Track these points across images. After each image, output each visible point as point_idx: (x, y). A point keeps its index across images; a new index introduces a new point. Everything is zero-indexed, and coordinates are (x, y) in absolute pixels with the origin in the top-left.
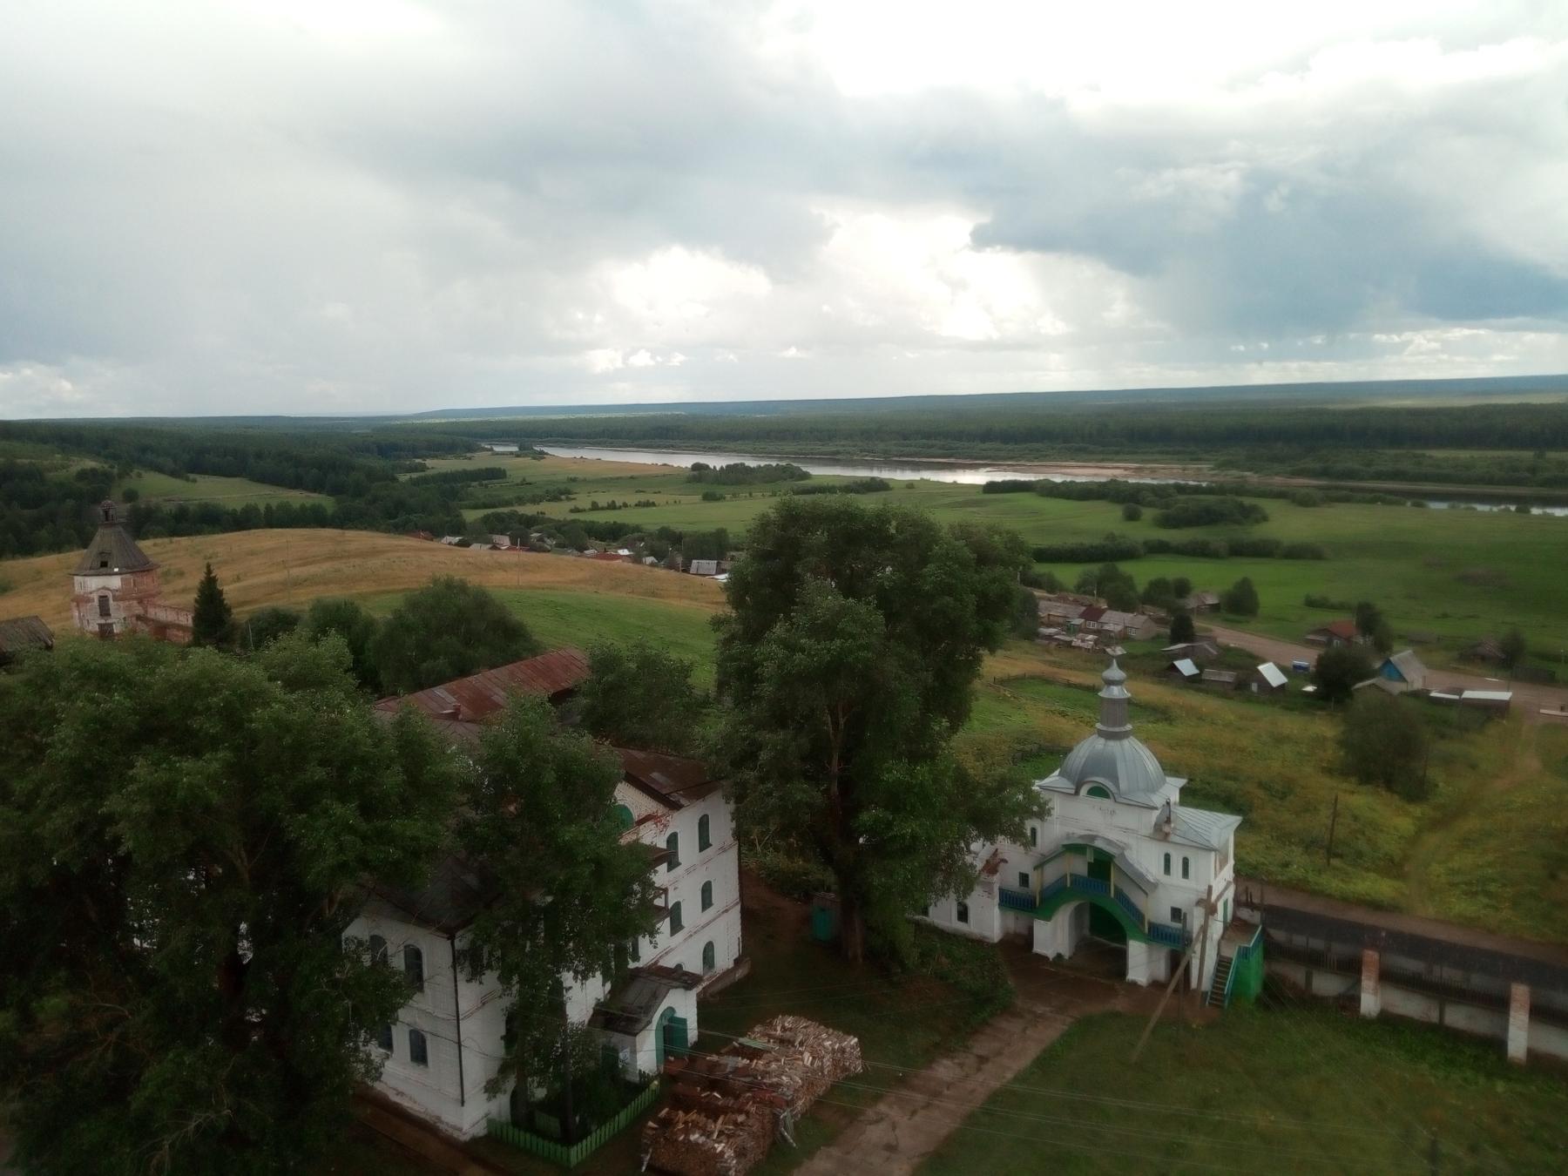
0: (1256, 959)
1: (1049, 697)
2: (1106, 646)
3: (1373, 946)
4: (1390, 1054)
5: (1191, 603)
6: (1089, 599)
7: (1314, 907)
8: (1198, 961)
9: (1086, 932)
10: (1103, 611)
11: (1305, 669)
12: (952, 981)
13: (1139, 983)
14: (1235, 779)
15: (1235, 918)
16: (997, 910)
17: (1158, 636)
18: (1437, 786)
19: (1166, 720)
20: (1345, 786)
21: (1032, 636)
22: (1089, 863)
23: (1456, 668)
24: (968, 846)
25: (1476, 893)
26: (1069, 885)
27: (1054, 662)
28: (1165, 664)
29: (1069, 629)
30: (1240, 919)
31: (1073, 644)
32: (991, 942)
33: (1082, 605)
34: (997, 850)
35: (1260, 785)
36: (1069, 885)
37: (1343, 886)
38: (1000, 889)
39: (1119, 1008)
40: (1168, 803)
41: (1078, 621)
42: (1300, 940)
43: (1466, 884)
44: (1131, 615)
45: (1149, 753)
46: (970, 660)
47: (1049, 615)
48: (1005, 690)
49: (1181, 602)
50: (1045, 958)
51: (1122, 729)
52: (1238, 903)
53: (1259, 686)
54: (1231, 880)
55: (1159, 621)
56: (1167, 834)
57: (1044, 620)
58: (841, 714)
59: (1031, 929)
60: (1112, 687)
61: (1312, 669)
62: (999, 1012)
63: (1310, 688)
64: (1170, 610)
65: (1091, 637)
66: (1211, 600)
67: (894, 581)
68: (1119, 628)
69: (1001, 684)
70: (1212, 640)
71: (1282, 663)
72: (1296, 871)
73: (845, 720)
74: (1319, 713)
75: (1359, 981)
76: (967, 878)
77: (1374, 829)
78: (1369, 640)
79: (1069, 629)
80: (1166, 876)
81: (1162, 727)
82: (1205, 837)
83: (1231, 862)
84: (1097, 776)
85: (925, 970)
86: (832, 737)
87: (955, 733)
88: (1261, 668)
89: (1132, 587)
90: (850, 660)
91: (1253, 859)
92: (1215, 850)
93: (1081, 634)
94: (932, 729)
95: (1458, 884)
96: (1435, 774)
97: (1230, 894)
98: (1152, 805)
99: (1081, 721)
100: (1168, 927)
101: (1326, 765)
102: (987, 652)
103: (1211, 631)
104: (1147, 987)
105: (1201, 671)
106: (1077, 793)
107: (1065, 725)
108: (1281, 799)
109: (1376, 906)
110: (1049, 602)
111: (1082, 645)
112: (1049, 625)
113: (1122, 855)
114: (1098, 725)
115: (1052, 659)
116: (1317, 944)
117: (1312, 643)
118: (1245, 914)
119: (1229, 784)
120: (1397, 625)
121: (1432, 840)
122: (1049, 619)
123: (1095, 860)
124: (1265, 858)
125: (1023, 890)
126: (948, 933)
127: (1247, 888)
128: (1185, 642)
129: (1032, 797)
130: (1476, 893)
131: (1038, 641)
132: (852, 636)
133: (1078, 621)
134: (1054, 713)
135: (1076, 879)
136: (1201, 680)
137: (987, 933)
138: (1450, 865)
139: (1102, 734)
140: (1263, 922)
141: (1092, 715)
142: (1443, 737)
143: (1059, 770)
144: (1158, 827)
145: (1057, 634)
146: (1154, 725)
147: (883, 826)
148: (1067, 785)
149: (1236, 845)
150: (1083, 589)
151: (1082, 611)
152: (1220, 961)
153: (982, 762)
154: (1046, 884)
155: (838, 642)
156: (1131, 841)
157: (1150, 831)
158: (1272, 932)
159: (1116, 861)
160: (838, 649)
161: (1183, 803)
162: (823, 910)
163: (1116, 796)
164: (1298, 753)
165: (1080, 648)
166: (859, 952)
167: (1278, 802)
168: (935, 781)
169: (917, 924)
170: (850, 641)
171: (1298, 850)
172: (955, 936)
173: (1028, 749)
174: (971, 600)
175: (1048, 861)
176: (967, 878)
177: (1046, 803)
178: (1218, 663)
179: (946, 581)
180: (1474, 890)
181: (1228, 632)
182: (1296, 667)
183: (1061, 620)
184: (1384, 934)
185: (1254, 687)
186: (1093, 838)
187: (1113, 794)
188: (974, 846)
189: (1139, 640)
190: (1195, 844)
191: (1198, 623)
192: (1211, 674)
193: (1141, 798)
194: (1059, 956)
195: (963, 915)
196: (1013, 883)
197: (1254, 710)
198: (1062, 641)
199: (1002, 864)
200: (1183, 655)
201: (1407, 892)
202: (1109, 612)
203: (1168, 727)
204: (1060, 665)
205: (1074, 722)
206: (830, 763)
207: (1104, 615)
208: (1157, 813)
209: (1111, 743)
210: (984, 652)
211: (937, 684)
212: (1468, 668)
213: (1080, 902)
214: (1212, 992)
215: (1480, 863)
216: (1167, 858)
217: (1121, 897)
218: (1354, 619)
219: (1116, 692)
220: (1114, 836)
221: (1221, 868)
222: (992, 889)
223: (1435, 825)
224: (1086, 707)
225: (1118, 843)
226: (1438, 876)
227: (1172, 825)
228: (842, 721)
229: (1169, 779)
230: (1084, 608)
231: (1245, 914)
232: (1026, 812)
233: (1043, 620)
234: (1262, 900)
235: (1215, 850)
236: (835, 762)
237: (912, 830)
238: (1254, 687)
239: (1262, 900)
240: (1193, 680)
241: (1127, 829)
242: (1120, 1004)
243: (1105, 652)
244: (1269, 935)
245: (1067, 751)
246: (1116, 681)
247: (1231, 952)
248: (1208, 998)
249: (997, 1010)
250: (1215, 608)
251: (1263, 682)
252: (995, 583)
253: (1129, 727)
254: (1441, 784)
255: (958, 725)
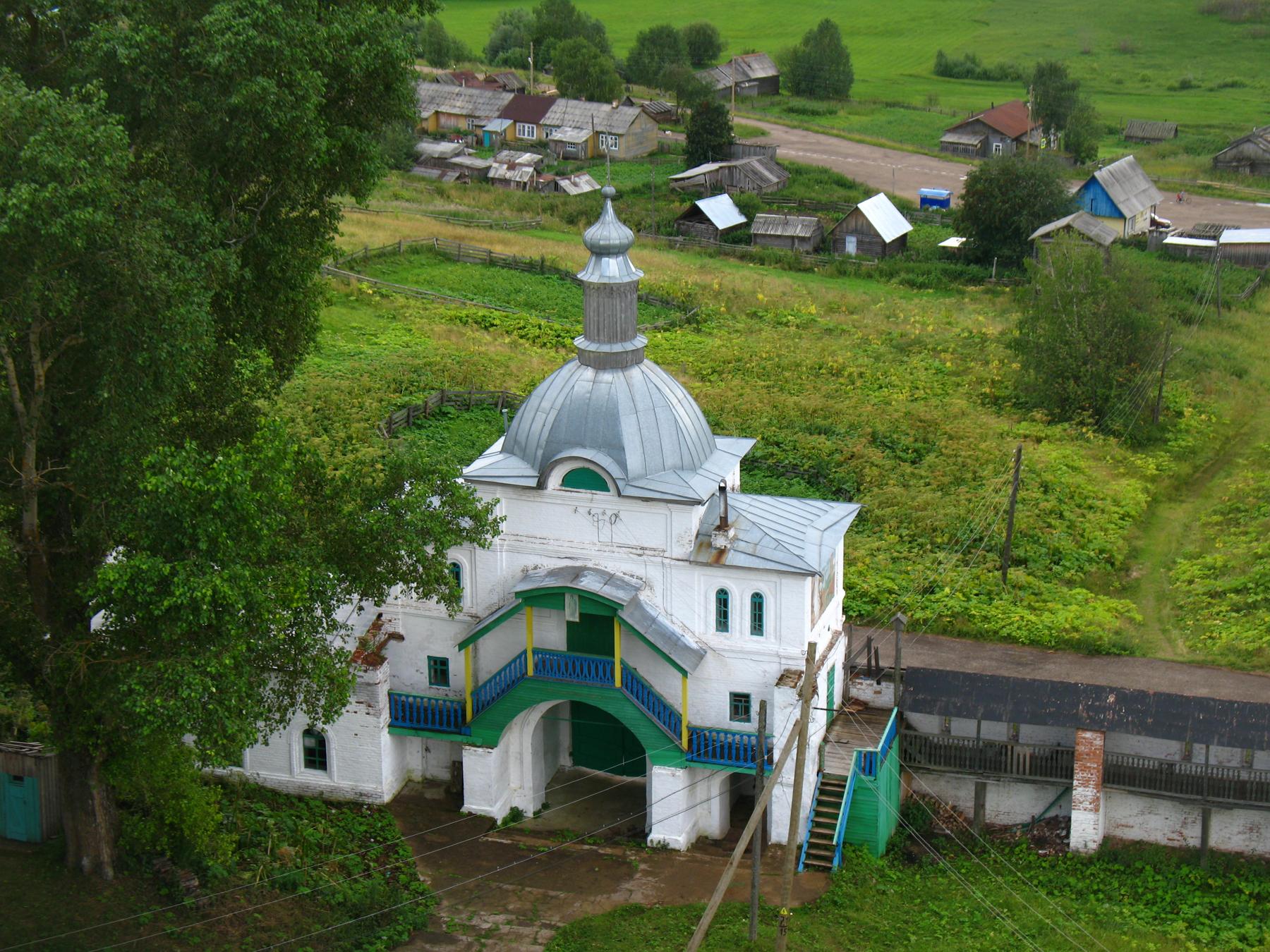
0: (889, 768)
1: (452, 289)
2: (557, 174)
3: (1095, 726)
4: (1121, 913)
5: (723, 77)
6: (518, 77)
7: (982, 662)
8: (789, 792)
9: (566, 761)
10: (551, 101)
11: (944, 203)
12: (307, 891)
13: (672, 846)
14: (826, 432)
15: (847, 699)
16: (385, 738)
17: (662, 150)
18: (1180, 414)
19: (689, 322)
20: (1024, 428)
21: (407, 160)
22: (570, 624)
23: (1207, 187)
24: (328, 612)
25: (1255, 606)
26: (530, 672)
27: (455, 215)
28: (679, 207)
29: (480, 142)
30: (857, 702)
31: (491, 174)
32: (378, 801)
33: (504, 88)
34: (380, 615)
35: (874, 439)
36: (530, 672)
37: (1033, 618)
38: (390, 695)
39: (637, 898)
40: (722, 490)
41: (498, 125)
42: (964, 728)
43: (1237, 591)
44: (606, 108)
45: (680, 392)
46: (314, 220)
47: (437, 113)
48: (360, 280)
49: (702, 76)
50: (486, 823)
51: (629, 346)
52: (852, 671)
53: (860, 244)
54: (840, 628)
55: (664, 118)
56: (722, 552)
57: (430, 126)
58: (36, 354)
59: (457, 768)
60: (605, 260)
61: (955, 204)
62: (405, 937)
63: (954, 242)
64: (684, 94)
65: (527, 157)
66: (762, 71)
67: (138, 45)
68: (582, 136)
69: (352, 269)
70: (766, 151)
71: (899, 193)
72: (948, 600)
73: (48, 364)
74: (971, 288)
75: (1069, 789)
76: (331, 680)
77: (1079, 506)
78: (1057, 137)
79: (480, 142)
80: (755, 638)
81: (682, 337)
82: (792, 549)
83: (840, 594)
84: (584, 447)
85: (247, 875)
86: (20, 406)
87: (287, 378)
88: (865, 206)
89: (604, 49)
90: (55, 229)
91: (870, 584)
92: (813, 574)
93: (505, 153)
94: (238, 373)
95: (1224, 593)
96: (1178, 393)
97: (838, 657)
98: (697, 497)
99: (522, 337)
100: (726, 732)
101: (988, 390)
102: (348, 200)
103: (763, 133)
104: (688, 850)
105: (751, 219)
106: (541, 485)
107: (490, 346)
108: (913, 462)
109: (1090, 649)
110: (435, 86)
111: (509, 175)
112: (440, 137)
113: (635, 602)
114: (580, 342)
115: (452, 207)
116: (995, 731)
117: (954, 150)
118: (865, 690)
119: (824, 444)
120: (1105, 109)
121: (1176, 514)
122: (438, 119)
123: (581, 615)
124: (893, 580)
125: (438, 692)
126: (288, 796)
127: (869, 640)
128: (714, 161)
129: (458, 500)
130: (1255, 606)
131: (419, 171)
132: (55, 175)
133: (498, 125)
134: (466, 323)
135: (545, 659)
136: (750, 236)
137: (368, 787)
138: (1209, 560)
139: (586, 359)
140: (899, 702)
141: (543, 322)
142: (1188, 321)
143: (502, 440)
144: (703, 541)
145: (457, 155)
146: (667, 334)
147: (150, 589)
148: (519, 470)
149: (849, 562)
150: (501, 55)
151: (506, 102)
152: (823, 784)
153: (325, 437)
154: (484, 677)
155: (24, 190)
156: (652, 572)
157: (685, 548)
158: (915, 718)
159: (624, 615)
160: (25, 207)
161: (745, 488)
162: (18, 779)
163: (620, 484)
164: (938, 371)
165: (505, 182)
166: (106, 854)
167: (908, 468)
168: (257, 484)
169: (221, 782)
170: (51, 186)
171: (949, 559)
172: (300, 798)
173: (420, 402)
174: (314, 82)
175: (486, 629)
176: (331, 680)
177: (488, 509)
178: (780, 201)
179: (258, 41)
180: (1250, 600)
181: (796, 136)
182: (925, 201)
183: (463, 125)
184: (1111, 699)
185: (851, 246)
186: (578, 573)
187: (614, 480)
188: (342, 614)
189: (624, 160)
190: (793, 570)
191: (740, 120)
192: (767, 224)
193: (673, 487)
194: (516, 814)
195: (317, 756)
196: (417, 680)
197: (855, 291)
198: (468, 167)
199: (393, 643)
200: (715, 189)
201: (1139, 617)
202: (561, 104)
203: (693, 337)
204: (468, 221)
205: (507, 340)
206: (19, 463)
207: (554, 108)
208: (701, 510)
209: (607, 377)
210: (343, 201)
211: (248, 274)
212: (1230, 186)
213: (544, 707)
214: (811, 846)
215: (1260, 551)
216: (723, 599)
217: (636, 685)
218: (1030, 98)
219: (613, 269)
220: (619, 565)
221: (823, 606)
222: (374, 696)
223: (1182, 487)
224: (530, 306)
225: (627, 578)
226: (1191, 582)
227: (731, 533)
228: (40, 370)
229: (721, 442)
230: (510, 96)
231: (865, 690)
232: (448, 533)
233: (425, 125)
234: (897, 659)
235: (813, 574)
236: (31, 460)
237: (215, 592)
238: (851, 246)
239: (897, 659)
240: (734, 235)
241: (642, 548)
242: (639, 890)
243: (557, 187)
244: (909, 727)
245: (509, 405)
246: (615, 247)
247: (844, 765)
248: (803, 856)
249: (400, 934)
250: (769, 86)
251: (868, 234)
252: (361, 43)
253: (641, 341)
254: (1188, 411)
255: (292, 361)
